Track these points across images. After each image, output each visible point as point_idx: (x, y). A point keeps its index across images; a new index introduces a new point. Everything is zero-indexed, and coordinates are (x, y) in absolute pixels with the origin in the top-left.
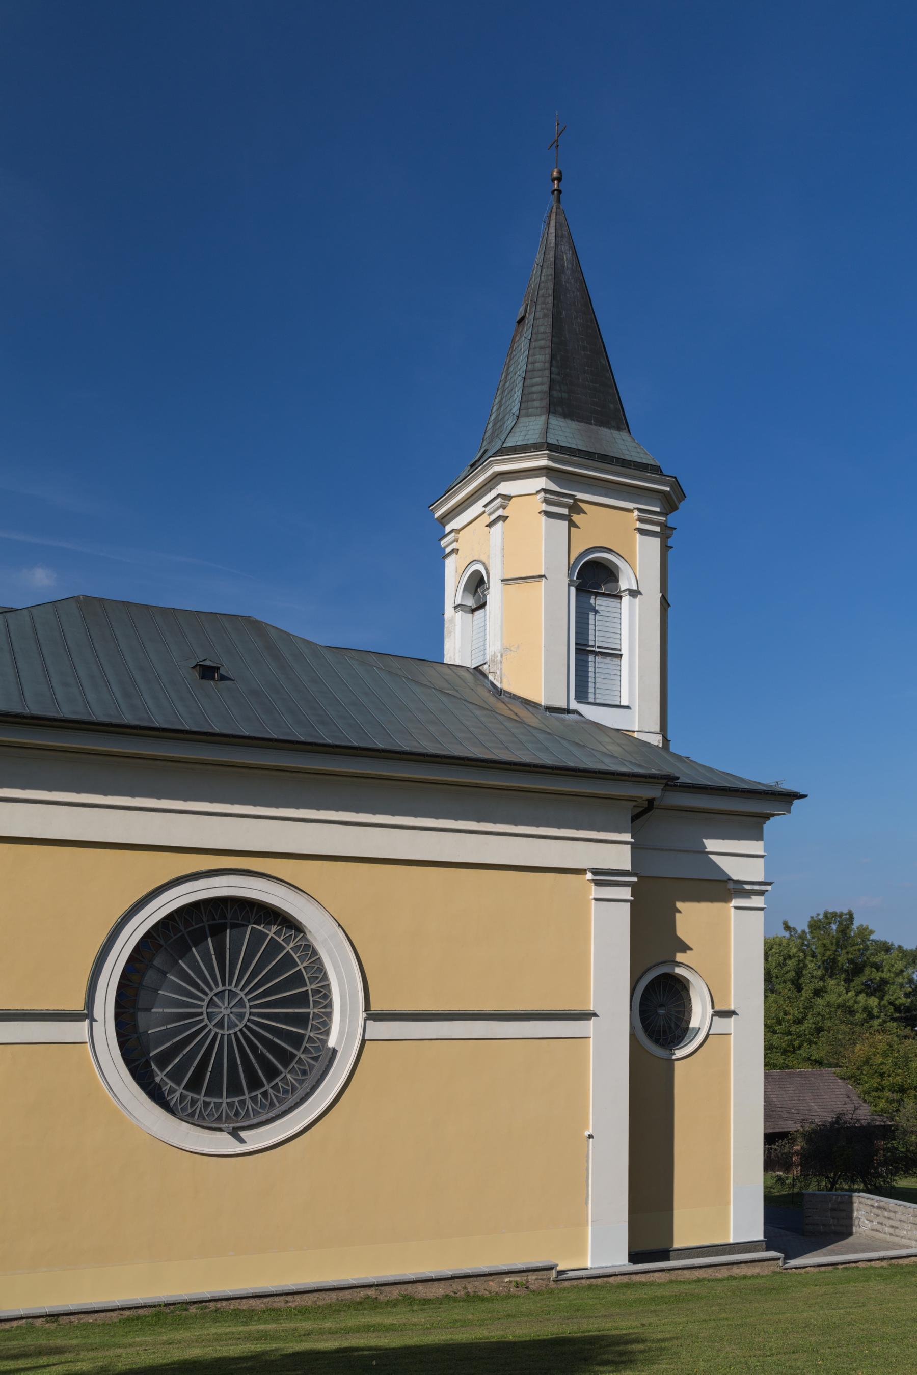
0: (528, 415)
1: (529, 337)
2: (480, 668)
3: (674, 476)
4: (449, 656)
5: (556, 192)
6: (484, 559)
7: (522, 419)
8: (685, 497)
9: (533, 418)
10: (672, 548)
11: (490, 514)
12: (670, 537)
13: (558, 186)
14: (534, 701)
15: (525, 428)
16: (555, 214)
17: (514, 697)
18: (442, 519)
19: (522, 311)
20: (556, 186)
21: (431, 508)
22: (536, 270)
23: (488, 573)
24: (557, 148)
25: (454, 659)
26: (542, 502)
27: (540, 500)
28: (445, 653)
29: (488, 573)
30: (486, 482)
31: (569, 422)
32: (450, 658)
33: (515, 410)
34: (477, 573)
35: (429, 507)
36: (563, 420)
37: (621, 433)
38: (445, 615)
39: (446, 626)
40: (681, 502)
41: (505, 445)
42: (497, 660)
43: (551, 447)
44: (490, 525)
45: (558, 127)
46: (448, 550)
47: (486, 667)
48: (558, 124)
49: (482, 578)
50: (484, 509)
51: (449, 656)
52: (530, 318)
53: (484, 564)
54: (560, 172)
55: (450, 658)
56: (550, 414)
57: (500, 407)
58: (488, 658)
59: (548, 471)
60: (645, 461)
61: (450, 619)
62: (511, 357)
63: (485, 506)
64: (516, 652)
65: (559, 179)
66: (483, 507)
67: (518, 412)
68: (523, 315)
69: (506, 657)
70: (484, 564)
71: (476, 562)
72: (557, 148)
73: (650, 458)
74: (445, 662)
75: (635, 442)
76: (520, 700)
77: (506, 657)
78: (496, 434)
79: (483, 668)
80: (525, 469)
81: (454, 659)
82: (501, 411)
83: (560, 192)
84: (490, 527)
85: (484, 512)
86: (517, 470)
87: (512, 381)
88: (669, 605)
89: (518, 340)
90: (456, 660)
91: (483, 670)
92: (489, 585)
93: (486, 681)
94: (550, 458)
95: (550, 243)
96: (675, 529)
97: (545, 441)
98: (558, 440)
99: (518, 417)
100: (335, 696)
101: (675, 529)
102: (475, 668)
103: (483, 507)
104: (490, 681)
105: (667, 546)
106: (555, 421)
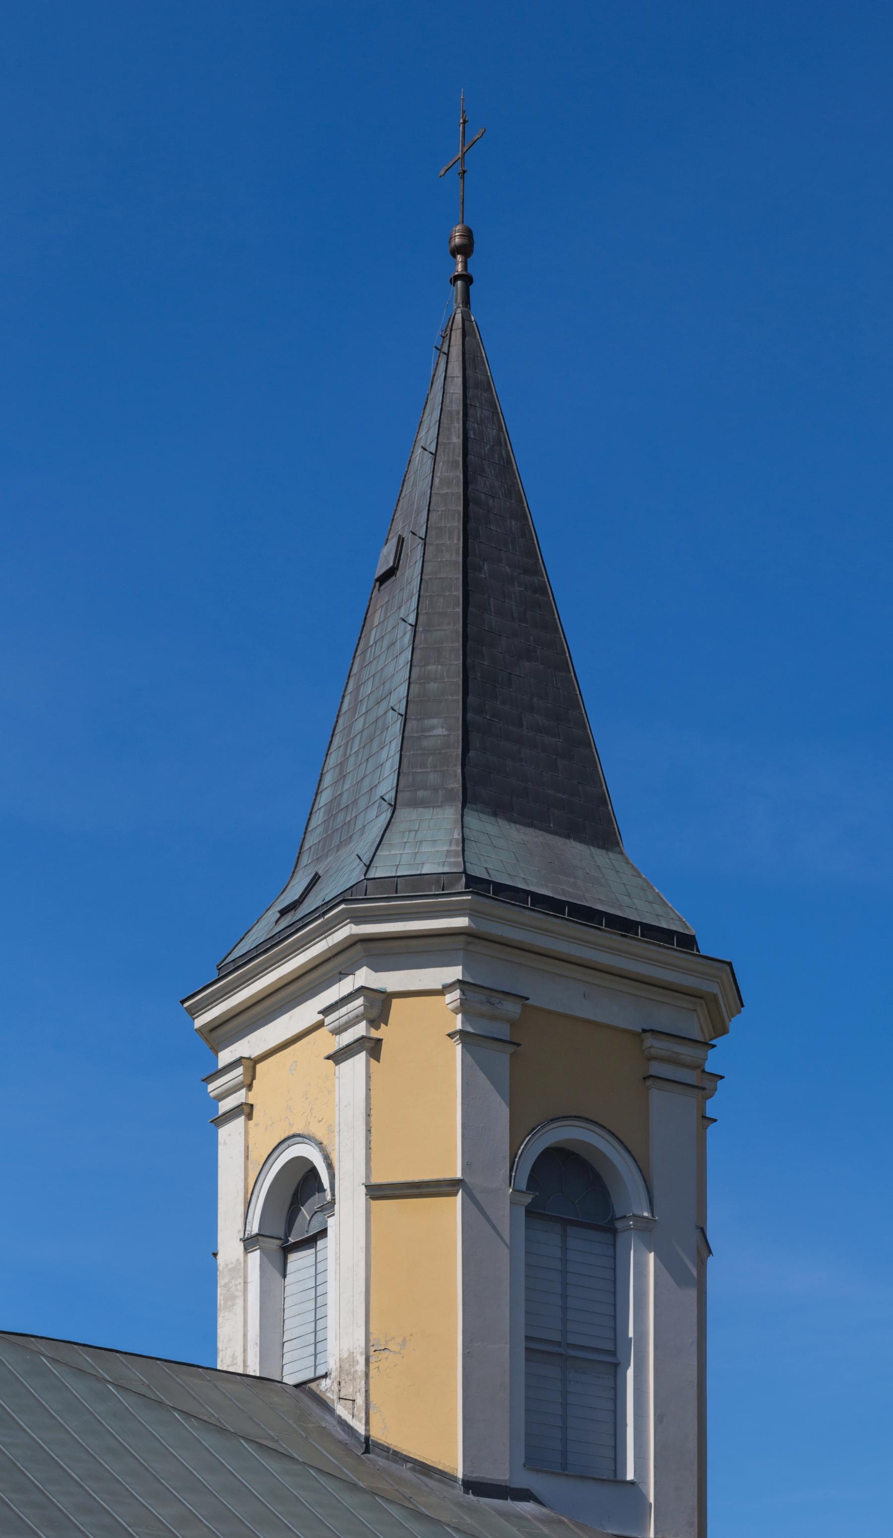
0: (415, 804)
1: (412, 619)
2: (313, 1385)
3: (728, 960)
4: (229, 1352)
5: (459, 283)
6: (320, 1134)
7: (401, 813)
8: (742, 1006)
9: (427, 813)
10: (715, 1120)
11: (337, 1031)
12: (711, 1097)
13: (465, 267)
14: (440, 1467)
15: (413, 834)
16: (459, 332)
17: (398, 1457)
18: (213, 1030)
19: (389, 553)
20: (460, 268)
21: (187, 1004)
22: (421, 462)
23: (330, 1166)
24: (463, 178)
25: (245, 1361)
26: (455, 1011)
27: (450, 1006)
28: (220, 1345)
29: (330, 1166)
30: (329, 955)
31: (504, 824)
32: (234, 1357)
33: (386, 788)
34: (300, 1161)
35: (183, 1002)
36: (492, 819)
37: (610, 854)
38: (219, 1256)
39: (221, 1282)
40: (733, 1016)
41: (371, 875)
42: (356, 1371)
43: (476, 885)
44: (338, 1057)
45: (464, 128)
46: (225, 1106)
47: (324, 1384)
48: (465, 122)
49: (312, 1173)
50: (321, 1017)
51: (229, 1352)
52: (411, 573)
53: (319, 1144)
54: (468, 234)
55: (234, 1357)
56: (468, 805)
57: (342, 777)
58: (332, 1363)
59: (470, 939)
60: (664, 925)
61: (230, 1266)
62: (364, 660)
63: (326, 1011)
64: (400, 1353)
65: (466, 250)
66: (320, 1013)
67: (393, 793)
68: (391, 564)
69: (376, 1365)
70: (319, 1144)
71: (300, 1139)
72: (463, 178)
73: (672, 915)
74: (219, 1368)
75: (641, 877)
76: (410, 1465)
77: (376, 1365)
78: (336, 841)
79: (318, 1385)
80: (421, 934)
81: (245, 1361)
82: (346, 786)
83: (467, 279)
84: (337, 1063)
85: (320, 1025)
86: (402, 935)
87: (371, 717)
88: (710, 1252)
89: (381, 623)
90: (249, 1363)
91: (318, 1392)
92: (333, 1195)
93: (328, 1417)
94: (472, 913)
95: (451, 402)
96: (722, 1077)
97: (461, 870)
98: (486, 868)
99: (394, 808)
100: (51, 1456)
101: (722, 1077)
102: (297, 1386)
103: (320, 1013)
104: (340, 1417)
105: (704, 1117)
106: (479, 823)
